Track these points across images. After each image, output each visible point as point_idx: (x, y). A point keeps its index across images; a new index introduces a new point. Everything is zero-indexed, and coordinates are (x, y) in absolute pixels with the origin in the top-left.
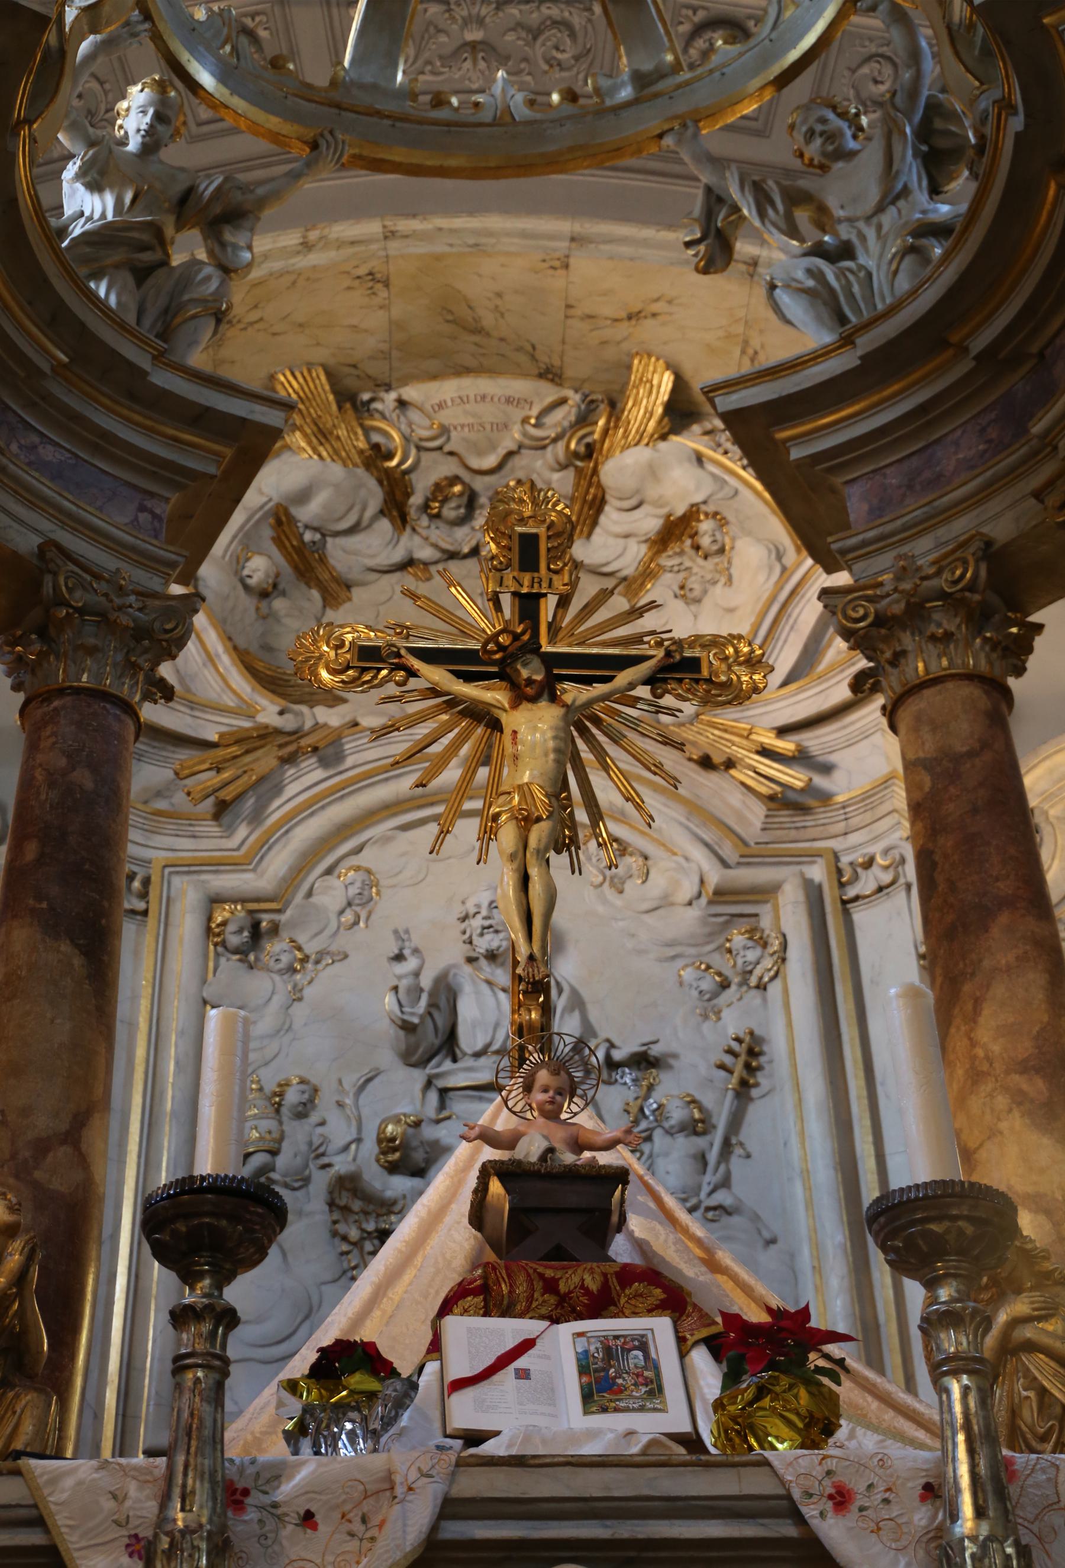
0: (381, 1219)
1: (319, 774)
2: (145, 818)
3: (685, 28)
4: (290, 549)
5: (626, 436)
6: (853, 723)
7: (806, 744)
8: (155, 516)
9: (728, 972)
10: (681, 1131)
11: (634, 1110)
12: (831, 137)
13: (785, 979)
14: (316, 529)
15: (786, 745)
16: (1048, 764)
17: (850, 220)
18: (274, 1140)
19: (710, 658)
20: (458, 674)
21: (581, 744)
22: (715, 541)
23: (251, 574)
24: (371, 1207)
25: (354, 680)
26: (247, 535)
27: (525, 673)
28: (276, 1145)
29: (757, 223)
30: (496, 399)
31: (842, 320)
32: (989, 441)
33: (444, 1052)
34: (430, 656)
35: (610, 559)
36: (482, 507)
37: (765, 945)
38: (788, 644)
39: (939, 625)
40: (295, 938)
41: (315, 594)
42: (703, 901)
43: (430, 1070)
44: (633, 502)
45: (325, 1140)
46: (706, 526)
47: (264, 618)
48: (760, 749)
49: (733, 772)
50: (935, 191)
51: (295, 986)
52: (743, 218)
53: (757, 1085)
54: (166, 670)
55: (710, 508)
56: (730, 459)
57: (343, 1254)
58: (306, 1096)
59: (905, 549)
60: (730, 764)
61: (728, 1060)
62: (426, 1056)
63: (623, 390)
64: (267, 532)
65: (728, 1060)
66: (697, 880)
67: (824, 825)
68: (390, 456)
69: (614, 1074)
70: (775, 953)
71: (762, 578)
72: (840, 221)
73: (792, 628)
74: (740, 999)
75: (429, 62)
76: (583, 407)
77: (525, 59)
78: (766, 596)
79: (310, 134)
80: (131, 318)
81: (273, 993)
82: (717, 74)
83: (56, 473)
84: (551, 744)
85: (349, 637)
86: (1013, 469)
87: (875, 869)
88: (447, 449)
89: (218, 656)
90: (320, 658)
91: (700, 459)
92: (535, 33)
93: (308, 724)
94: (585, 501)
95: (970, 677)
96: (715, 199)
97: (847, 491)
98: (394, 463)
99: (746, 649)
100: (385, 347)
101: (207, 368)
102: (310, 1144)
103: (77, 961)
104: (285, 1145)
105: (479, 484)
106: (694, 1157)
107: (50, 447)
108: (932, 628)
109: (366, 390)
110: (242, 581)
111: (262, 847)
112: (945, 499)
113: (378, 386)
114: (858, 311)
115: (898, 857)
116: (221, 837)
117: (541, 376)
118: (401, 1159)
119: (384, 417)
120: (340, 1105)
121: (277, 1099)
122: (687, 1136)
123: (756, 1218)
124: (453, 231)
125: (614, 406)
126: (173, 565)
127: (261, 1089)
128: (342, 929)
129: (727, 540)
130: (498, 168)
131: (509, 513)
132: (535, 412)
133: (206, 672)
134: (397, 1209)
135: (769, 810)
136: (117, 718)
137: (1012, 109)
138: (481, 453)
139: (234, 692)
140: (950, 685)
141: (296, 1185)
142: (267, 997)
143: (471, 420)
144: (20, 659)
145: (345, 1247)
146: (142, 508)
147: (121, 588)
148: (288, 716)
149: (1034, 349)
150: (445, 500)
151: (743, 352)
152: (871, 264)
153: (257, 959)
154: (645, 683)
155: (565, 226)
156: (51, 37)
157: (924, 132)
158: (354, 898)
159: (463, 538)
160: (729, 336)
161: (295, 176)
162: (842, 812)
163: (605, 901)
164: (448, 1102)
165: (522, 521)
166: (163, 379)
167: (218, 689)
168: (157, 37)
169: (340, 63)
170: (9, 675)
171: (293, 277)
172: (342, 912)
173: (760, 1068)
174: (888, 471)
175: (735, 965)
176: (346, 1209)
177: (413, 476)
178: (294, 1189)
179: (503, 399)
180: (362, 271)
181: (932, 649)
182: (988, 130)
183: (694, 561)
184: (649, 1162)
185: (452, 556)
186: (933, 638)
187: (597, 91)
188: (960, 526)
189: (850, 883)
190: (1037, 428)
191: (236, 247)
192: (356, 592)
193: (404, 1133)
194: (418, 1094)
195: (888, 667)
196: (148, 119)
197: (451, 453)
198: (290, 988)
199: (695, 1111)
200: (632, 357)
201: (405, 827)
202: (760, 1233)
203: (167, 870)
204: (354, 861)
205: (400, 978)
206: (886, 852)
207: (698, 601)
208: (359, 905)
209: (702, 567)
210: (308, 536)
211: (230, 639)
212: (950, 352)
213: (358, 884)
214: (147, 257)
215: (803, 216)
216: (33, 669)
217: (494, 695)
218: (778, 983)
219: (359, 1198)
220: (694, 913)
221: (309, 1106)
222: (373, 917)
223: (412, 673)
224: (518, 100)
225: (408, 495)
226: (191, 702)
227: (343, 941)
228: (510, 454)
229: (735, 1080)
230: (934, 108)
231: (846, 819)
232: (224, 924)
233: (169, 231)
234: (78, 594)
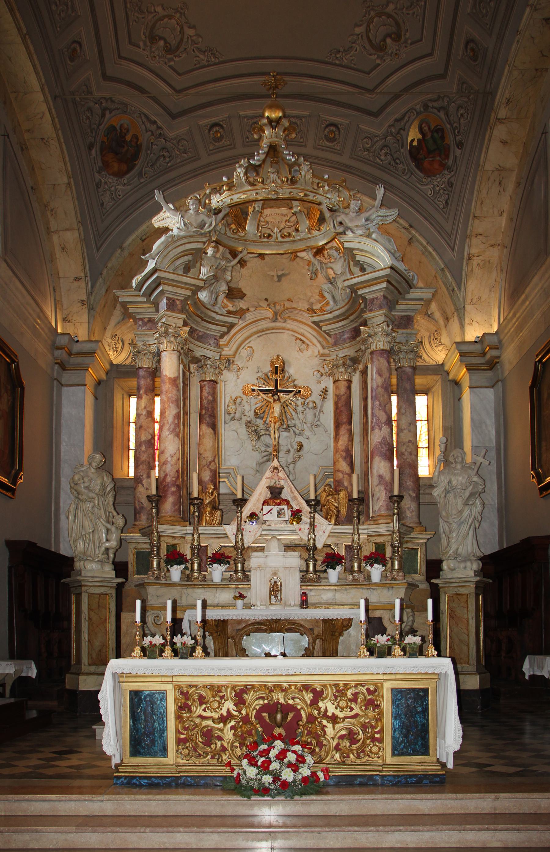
3: (324, 126)
45: (244, 410)
61: (321, 394)
65: (321, 394)
103: (212, 431)
143: (273, 220)
201: (259, 337)
204: (248, 345)
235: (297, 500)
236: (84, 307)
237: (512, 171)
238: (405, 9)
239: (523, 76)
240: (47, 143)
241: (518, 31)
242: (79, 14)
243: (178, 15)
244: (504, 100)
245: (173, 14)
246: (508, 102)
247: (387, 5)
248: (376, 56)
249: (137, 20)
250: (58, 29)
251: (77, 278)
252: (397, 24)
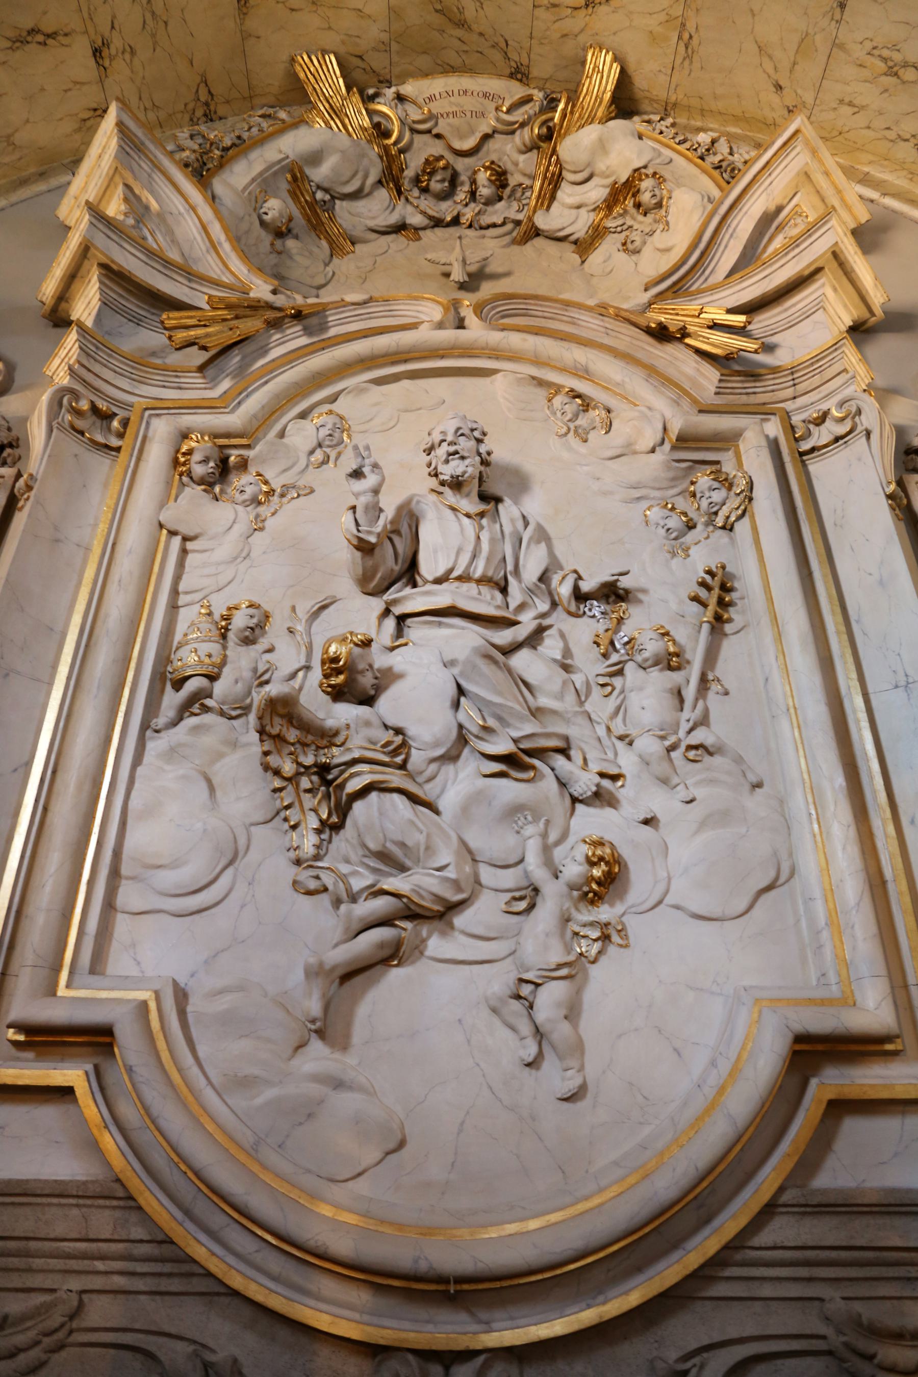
0: (322, 752)
2: (133, 368)
4: (304, 203)
6: (794, 305)
9: (692, 514)
10: (656, 664)
11: (604, 642)
13: (752, 518)
14: (326, 190)
18: (213, 665)
22: (654, 196)
23: (267, 211)
24: (310, 738)
26: (265, 181)
28: (216, 670)
30: (475, 94)
33: (404, 580)
35: (565, 225)
36: (462, 184)
37: (730, 487)
38: (728, 249)
40: (262, 472)
41: (324, 244)
42: (667, 446)
43: (389, 596)
48: (711, 324)
51: (257, 516)
53: (730, 620)
56: (664, 137)
57: (275, 791)
58: (255, 620)
62: (386, 583)
65: (703, 593)
66: (660, 427)
67: (773, 391)
69: (582, 606)
70: (742, 492)
73: (731, 236)
74: (708, 538)
76: (545, 103)
81: (234, 522)
87: (828, 423)
88: (434, 132)
89: (220, 244)
94: (545, 177)
100: (385, 37)
102: (255, 670)
104: (226, 670)
105: (460, 164)
106: (671, 691)
109: (372, 87)
111: (240, 394)
113: (381, 82)
115: (854, 410)
116: (205, 389)
117: (512, 76)
118: (346, 683)
120: (291, 632)
121: (223, 623)
122: (661, 670)
123: (739, 760)
127: (210, 614)
128: (311, 467)
129: (665, 192)
133: (209, 258)
134: (339, 740)
135: (722, 375)
138: (462, 137)
141: (234, 713)
142: (229, 525)
143: (454, 109)
145: (278, 783)
150: (431, 174)
153: (222, 491)
158: (324, 440)
159: (446, 209)
162: (790, 378)
163: (570, 449)
164: (406, 630)
167: (204, 248)
172: (312, 452)
173: (730, 604)
175: (698, 509)
176: (279, 739)
178: (231, 718)
179: (481, 94)
183: (634, 219)
184: (622, 697)
185: (437, 223)
189: (802, 438)
193: (350, 653)
194: (374, 621)
197: (438, 136)
198: (252, 517)
199: (670, 643)
200: (585, 50)
201: (379, 382)
202: (745, 775)
203: (147, 413)
205: (357, 495)
206: (841, 405)
208: (329, 446)
209: (642, 223)
210: (319, 195)
213: (329, 426)
218: (746, 520)
219: (295, 727)
220: (660, 457)
221: (257, 631)
222: (342, 458)
226: (189, 274)
227: (311, 478)
228: (486, 137)
229: (709, 615)
231: (794, 385)
232: (190, 452)
235: (444, 623)
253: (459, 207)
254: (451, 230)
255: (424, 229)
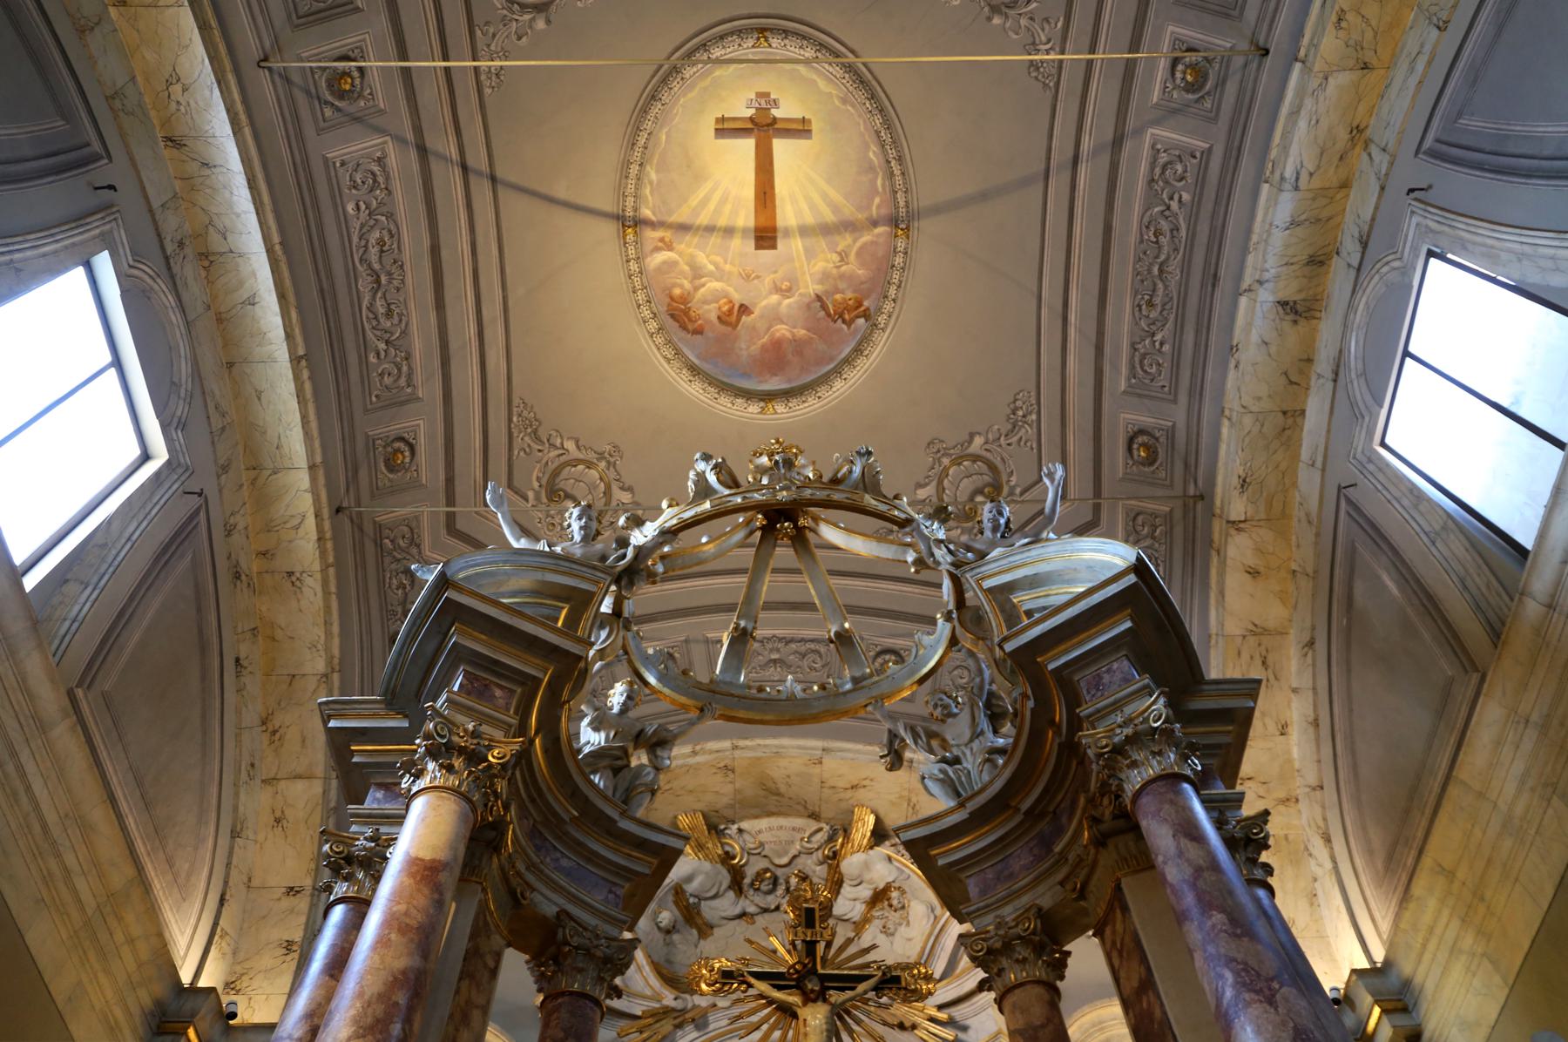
1: (695, 1034)
3: (872, 654)
5: (852, 847)
7: (953, 1014)
8: (616, 895)
12: (945, 707)
14: (695, 896)
15: (942, 1016)
16: (1078, 1023)
17: (958, 746)
19: (905, 975)
20: (774, 986)
21: (838, 1023)
25: (719, 990)
27: (810, 986)
29: (914, 747)
31: (958, 795)
32: (1035, 856)
34: (760, 976)
36: (781, 884)
39: (1020, 953)
41: (695, 932)
44: (858, 881)
46: (895, 894)
47: (668, 944)
49: (916, 1031)
50: (996, 732)
52: (907, 745)
54: (618, 981)
55: (896, 885)
59: (998, 912)
60: (914, 1027)
63: (850, 824)
64: (671, 898)
68: (734, 858)
71: (924, 922)
72: (952, 746)
75: (754, 668)
77: (799, 667)
78: (927, 932)
79: (700, 704)
80: (610, 793)
82: (890, 679)
83: (568, 873)
84: (824, 1027)
85: (717, 965)
86: (1048, 870)
88: (763, 854)
90: (701, 977)
91: (890, 859)
92: (804, 656)
93: (690, 1006)
95: (1038, 982)
96: (893, 735)
97: (968, 881)
98: (736, 861)
99: (924, 971)
101: (644, 818)
105: (779, 872)
107: (566, 860)
108: (1017, 956)
110: (657, 924)
112: (1016, 886)
114: (966, 791)
117: (809, 816)
119: (731, 837)
124: (765, 746)
125: (846, 832)
126: (624, 922)
130: (790, 720)
131: (800, 896)
132: (807, 835)
136: (591, 1008)
137: (1028, 698)
138: (780, 856)
139: (651, 987)
140: (1028, 987)
144: (543, 974)
146: (610, 891)
147: (597, 935)
148: (679, 1001)
149: (1051, 809)
150: (761, 882)
151: (908, 805)
152: (970, 767)
154: (872, 990)
155: (819, 744)
156: (582, 665)
157: (988, 705)
159: (771, 901)
160: (901, 797)
161: (692, 724)
165: (806, 901)
166: (625, 824)
168: (630, 662)
169: (714, 672)
170: (536, 983)
171: (687, 768)
174: (987, 870)
177: (746, 868)
180: (722, 765)
181: (1017, 967)
182: (1018, 706)
185: (766, 910)
186: (1017, 961)
187: (835, 685)
188: (1025, 900)
190: (1057, 849)
191: (663, 758)
192: (716, 930)
195: (996, 978)
196: (624, 698)
200: (854, 807)
207: (892, 934)
209: (894, 917)
210: (692, 900)
211: (650, 956)
212: (1010, 812)
214: (619, 763)
215: (935, 743)
216: (549, 980)
217: (793, 999)
223: (750, 986)
224: (798, 688)
225: (743, 878)
228: (795, 857)
230: (991, 694)
233: (631, 750)
234: (575, 938)
236: (289, 958)
237: (1282, 633)
238: (1002, 438)
239: (1262, 426)
240: (298, 583)
241: (1232, 349)
242: (421, 396)
243: (603, 464)
244: (1235, 481)
245: (595, 461)
246: (1244, 483)
247: (970, 442)
248: (959, 531)
249: (527, 450)
250: (374, 399)
251: (292, 888)
252: (992, 468)
253: (779, 899)
254: (775, 914)
255: (757, 914)
